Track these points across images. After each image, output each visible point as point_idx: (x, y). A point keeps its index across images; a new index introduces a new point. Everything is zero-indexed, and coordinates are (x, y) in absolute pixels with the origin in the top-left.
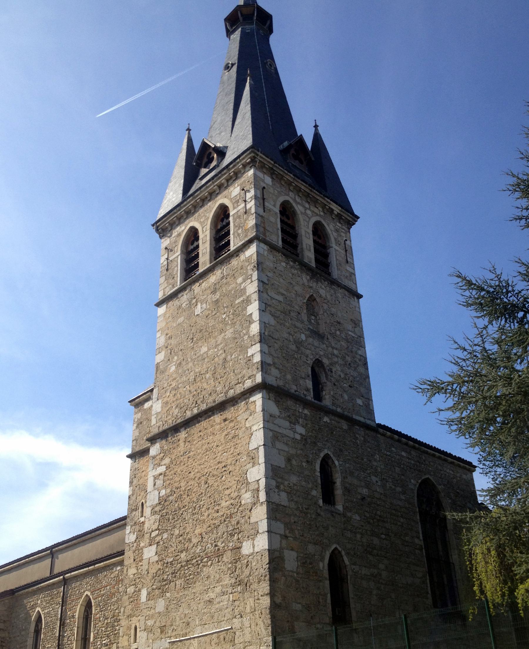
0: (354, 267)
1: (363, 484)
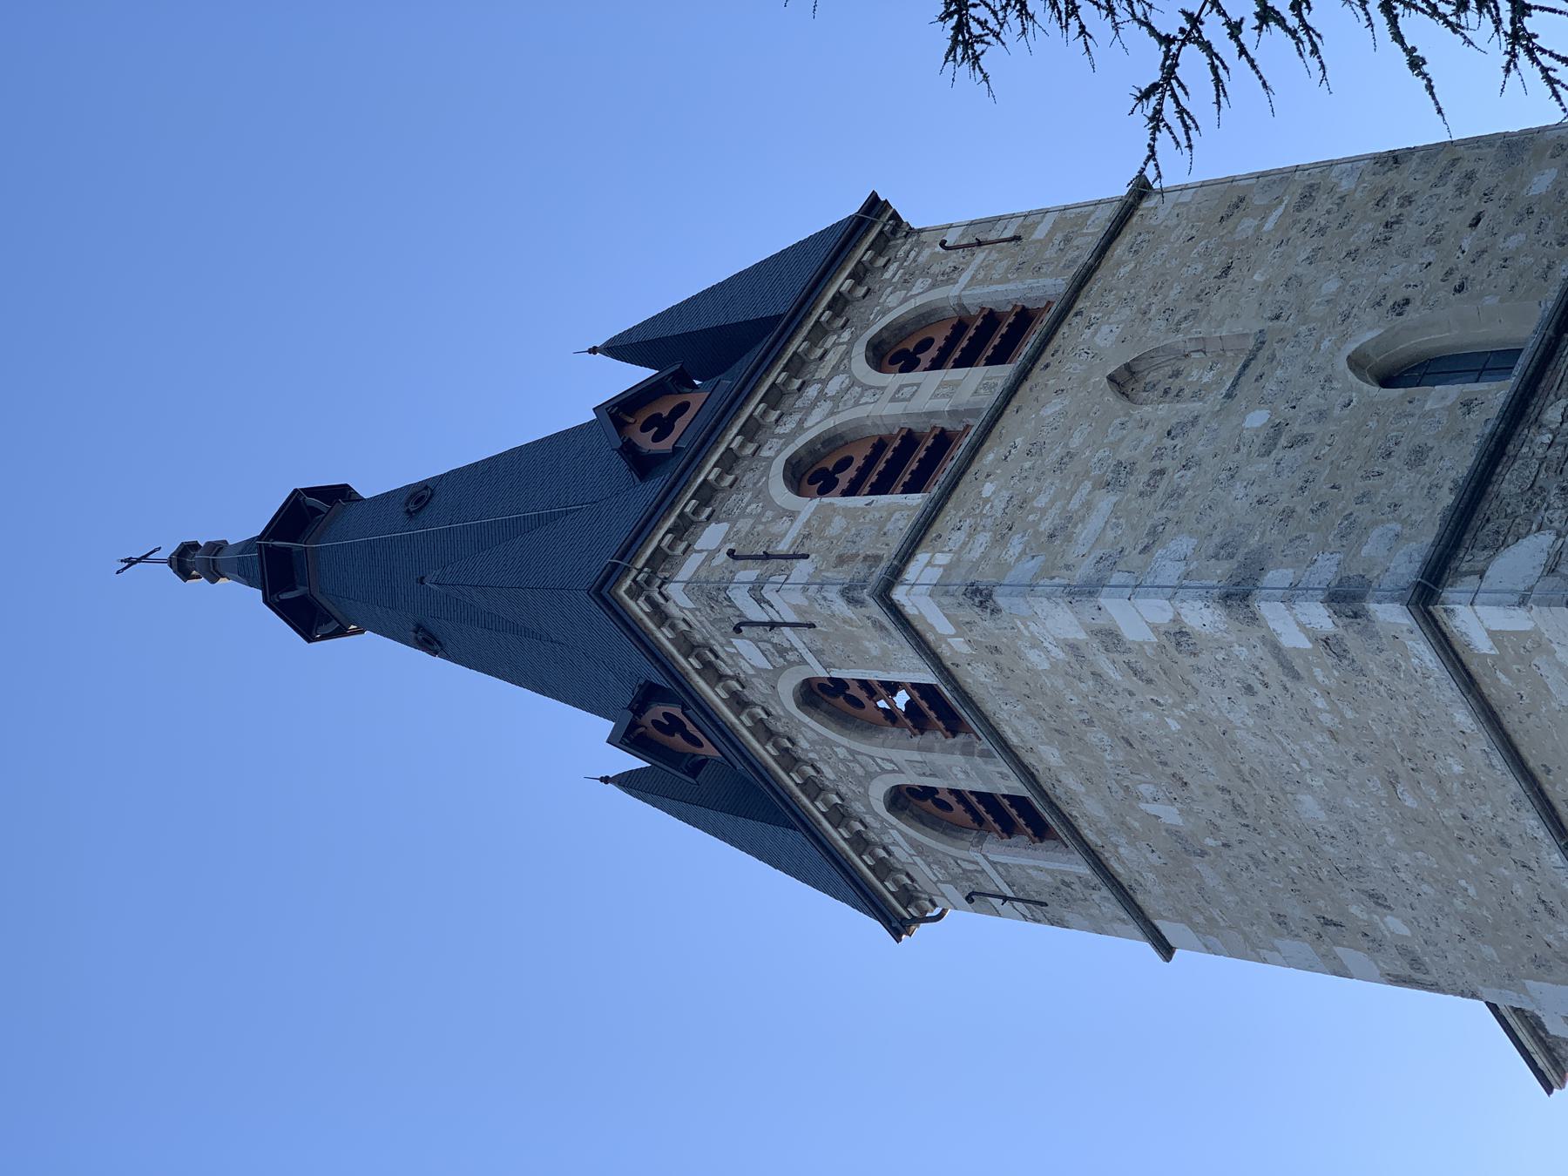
0: (1038, 212)
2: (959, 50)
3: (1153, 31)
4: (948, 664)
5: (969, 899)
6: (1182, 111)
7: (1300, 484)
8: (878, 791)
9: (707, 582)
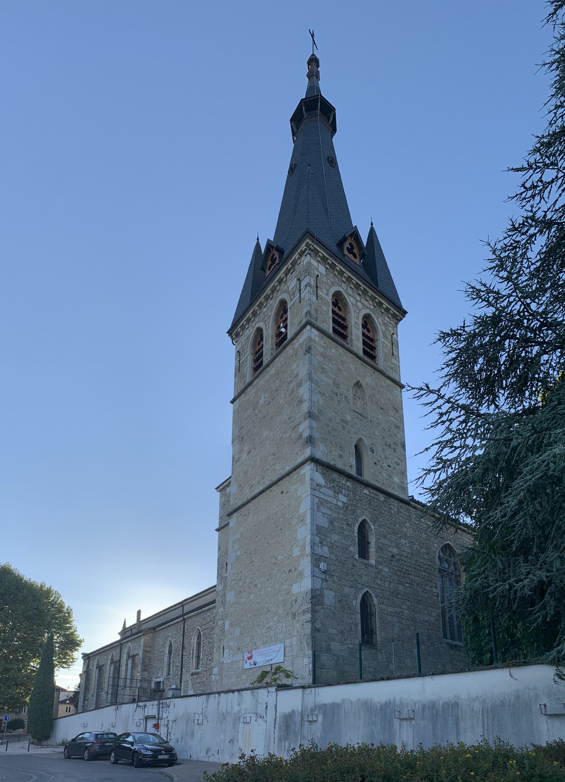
0: (399, 360)
1: (394, 544)
2: (442, 335)
3: (442, 387)
4: (292, 342)
5: (238, 352)
6: (422, 395)
7: (334, 428)
8: (261, 325)
9: (310, 269)
